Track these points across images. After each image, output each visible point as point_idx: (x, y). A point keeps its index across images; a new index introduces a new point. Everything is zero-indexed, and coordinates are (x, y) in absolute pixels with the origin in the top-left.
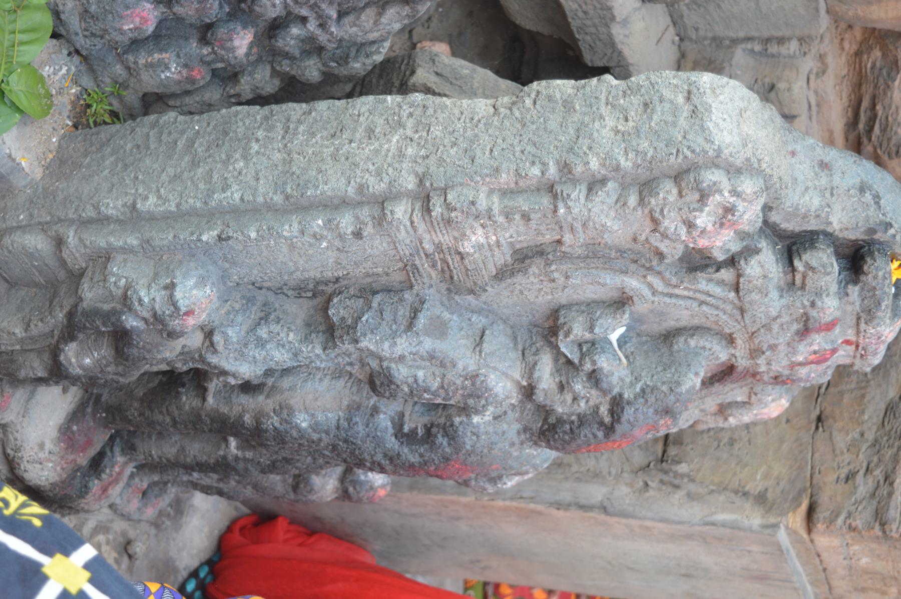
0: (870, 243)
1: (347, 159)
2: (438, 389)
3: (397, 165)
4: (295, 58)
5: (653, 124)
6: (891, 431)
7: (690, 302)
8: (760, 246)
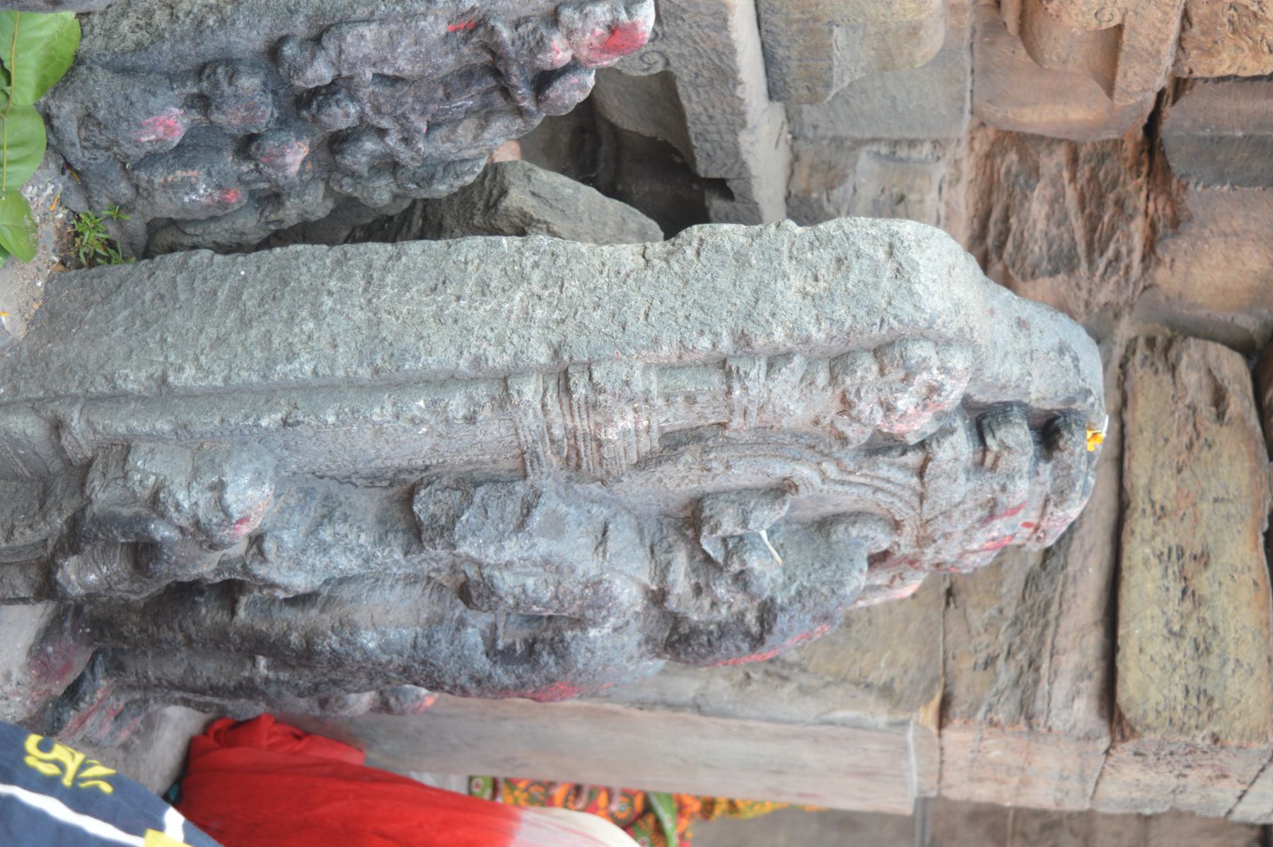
0: (1064, 413)
1: (456, 321)
2: (551, 599)
4: (360, 177)
5: (850, 286)
6: (1033, 605)
7: (864, 489)
8: (955, 425)
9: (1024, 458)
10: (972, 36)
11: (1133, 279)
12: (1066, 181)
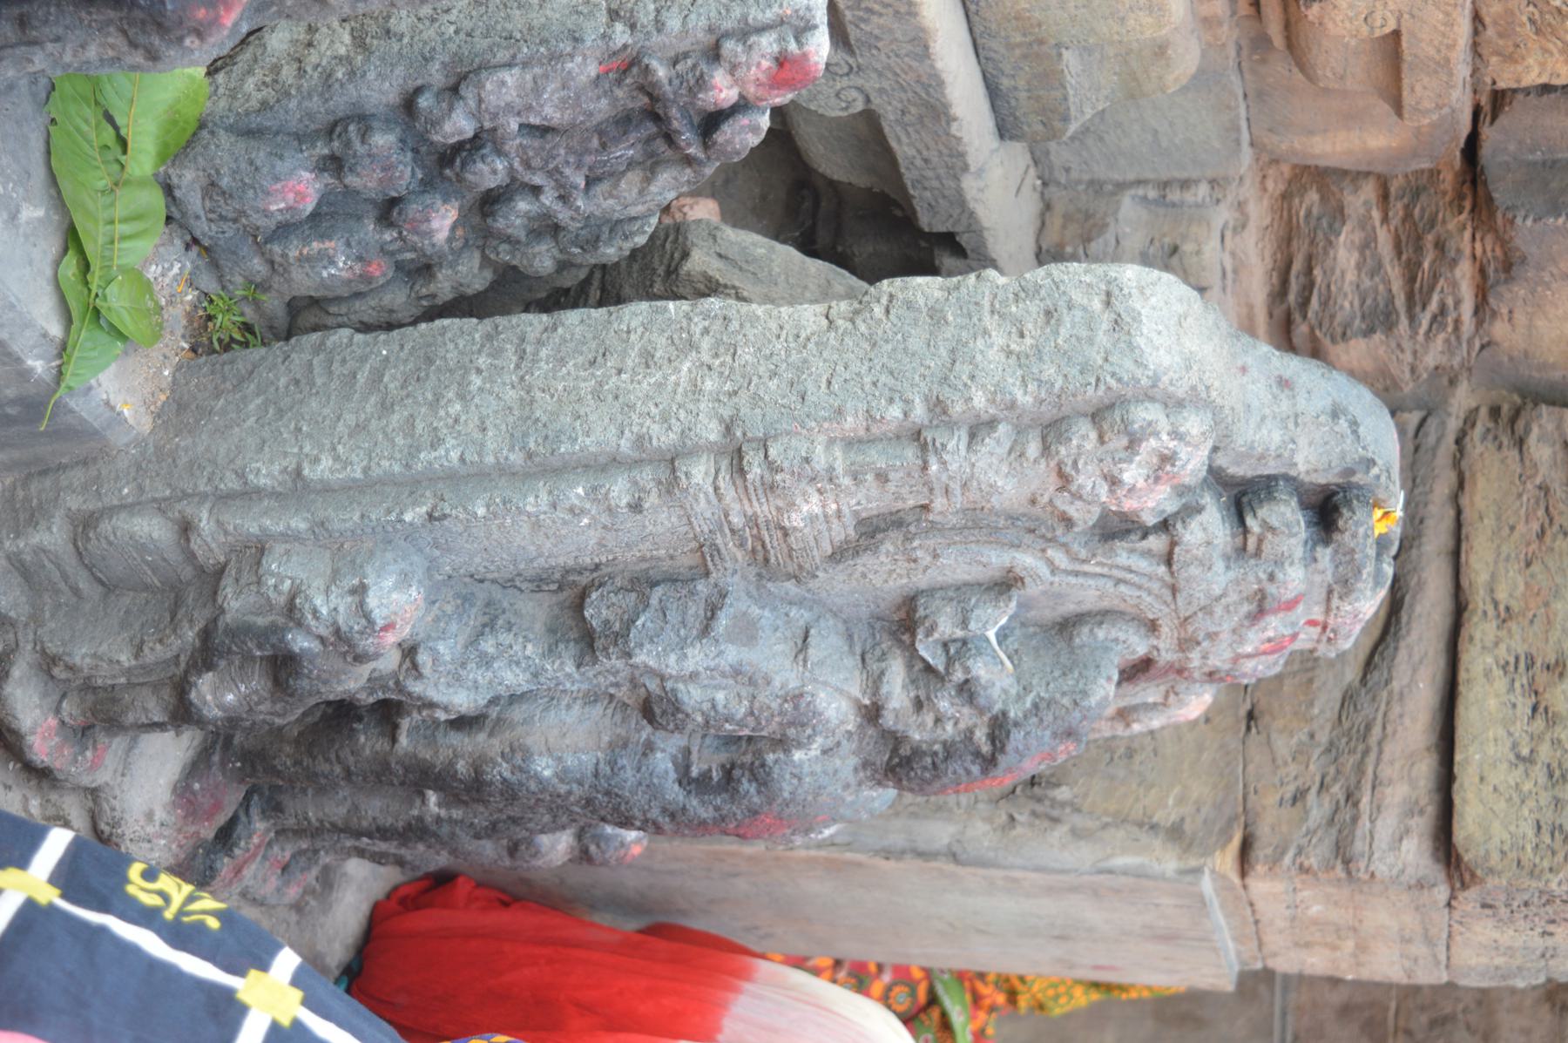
0: (1345, 488)
1: (616, 397)
2: (746, 716)
3: (691, 406)
4: (518, 242)
5: (1060, 341)
8: (1203, 502)
9: (1293, 541)
10: (1238, 54)
11: (1465, 337)
12: (1377, 223)
